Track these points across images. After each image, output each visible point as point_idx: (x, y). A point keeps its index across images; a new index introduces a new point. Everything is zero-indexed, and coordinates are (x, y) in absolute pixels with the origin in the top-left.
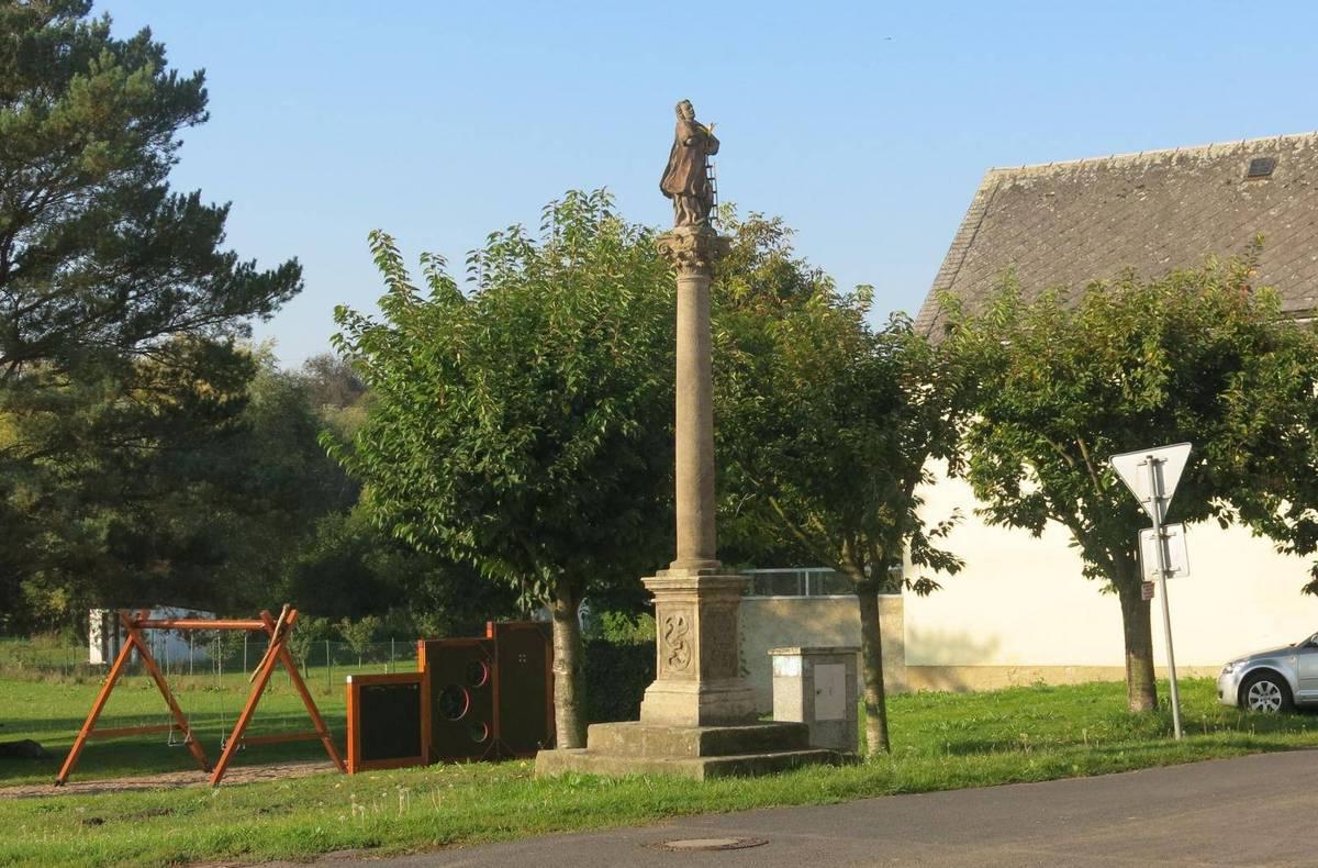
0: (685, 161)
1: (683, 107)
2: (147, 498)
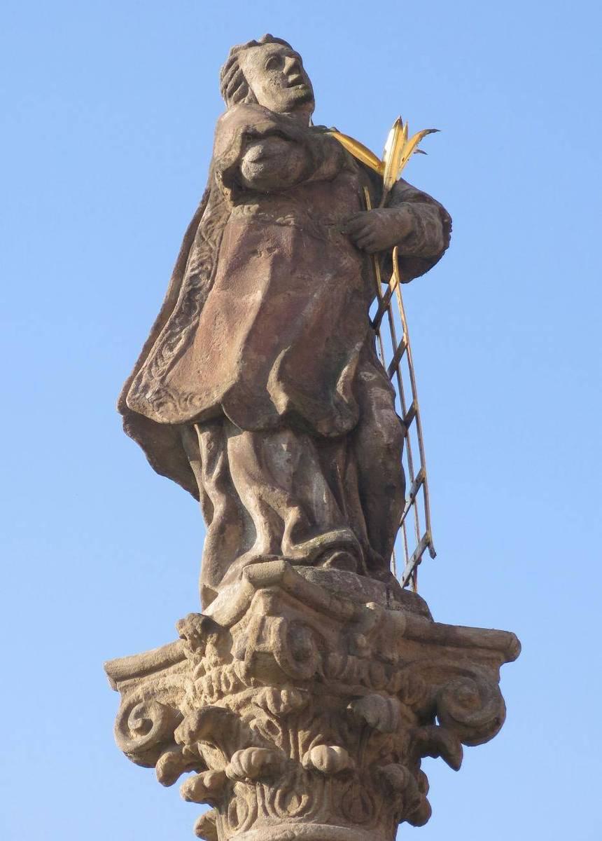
0: (239, 265)
1: (250, 64)
2: (419, 223)
